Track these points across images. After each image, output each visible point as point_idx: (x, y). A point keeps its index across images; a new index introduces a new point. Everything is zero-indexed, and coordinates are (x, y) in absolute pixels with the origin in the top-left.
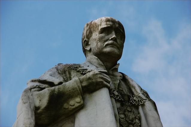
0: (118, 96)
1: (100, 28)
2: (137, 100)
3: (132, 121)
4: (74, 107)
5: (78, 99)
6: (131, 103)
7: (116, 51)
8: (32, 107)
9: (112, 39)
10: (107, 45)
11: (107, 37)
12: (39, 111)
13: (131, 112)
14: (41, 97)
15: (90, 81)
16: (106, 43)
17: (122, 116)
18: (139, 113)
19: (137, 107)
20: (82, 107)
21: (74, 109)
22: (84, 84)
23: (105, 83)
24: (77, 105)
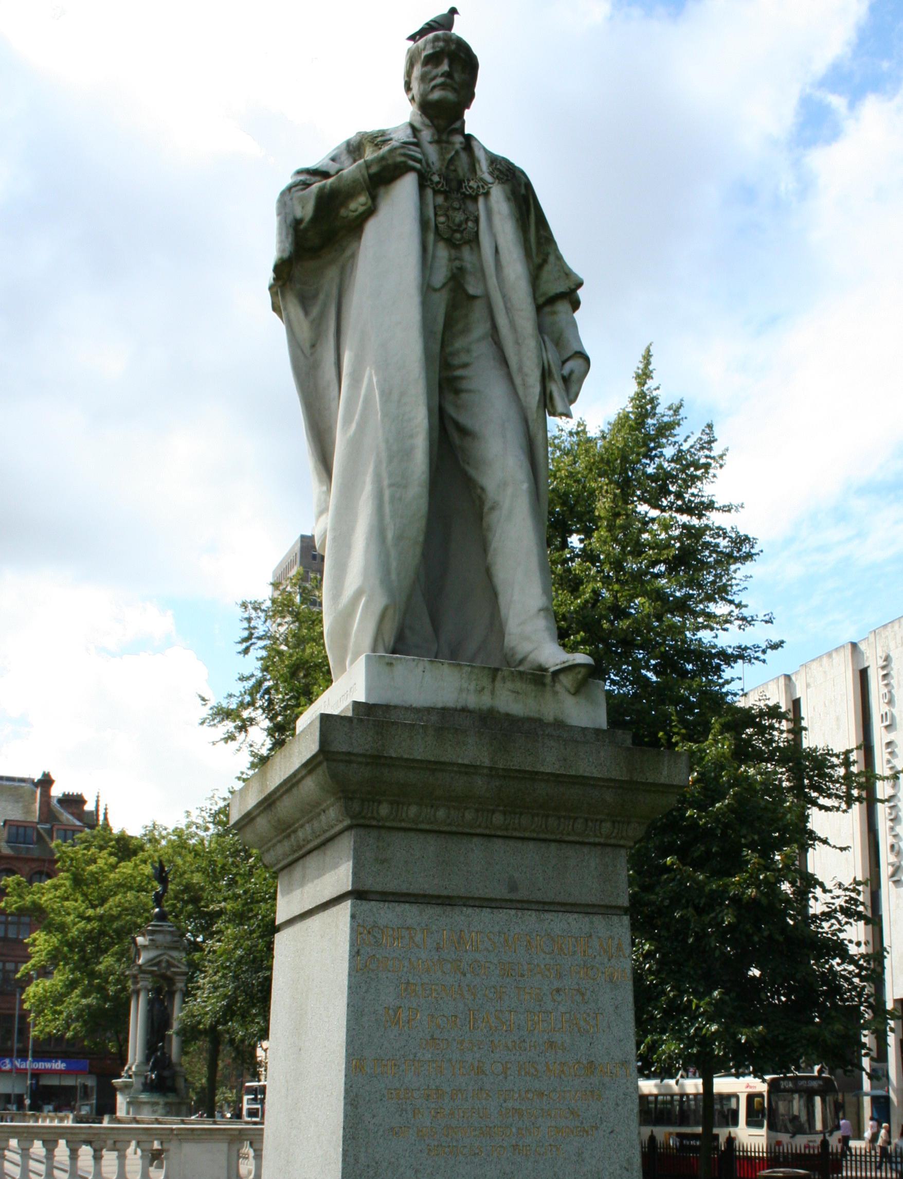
0: (438, 183)
1: (424, 54)
2: (475, 187)
3: (460, 225)
4: (357, 213)
5: (362, 199)
6: (464, 193)
7: (450, 96)
8: (288, 222)
9: (443, 75)
10: (434, 87)
11: (435, 72)
12: (302, 226)
13: (459, 209)
14: (303, 201)
15: (384, 163)
16: (433, 83)
17: (442, 219)
18: (478, 210)
19: (475, 199)
20: (370, 212)
21: (357, 217)
22: (374, 169)
23: (411, 163)
24: (361, 209)
